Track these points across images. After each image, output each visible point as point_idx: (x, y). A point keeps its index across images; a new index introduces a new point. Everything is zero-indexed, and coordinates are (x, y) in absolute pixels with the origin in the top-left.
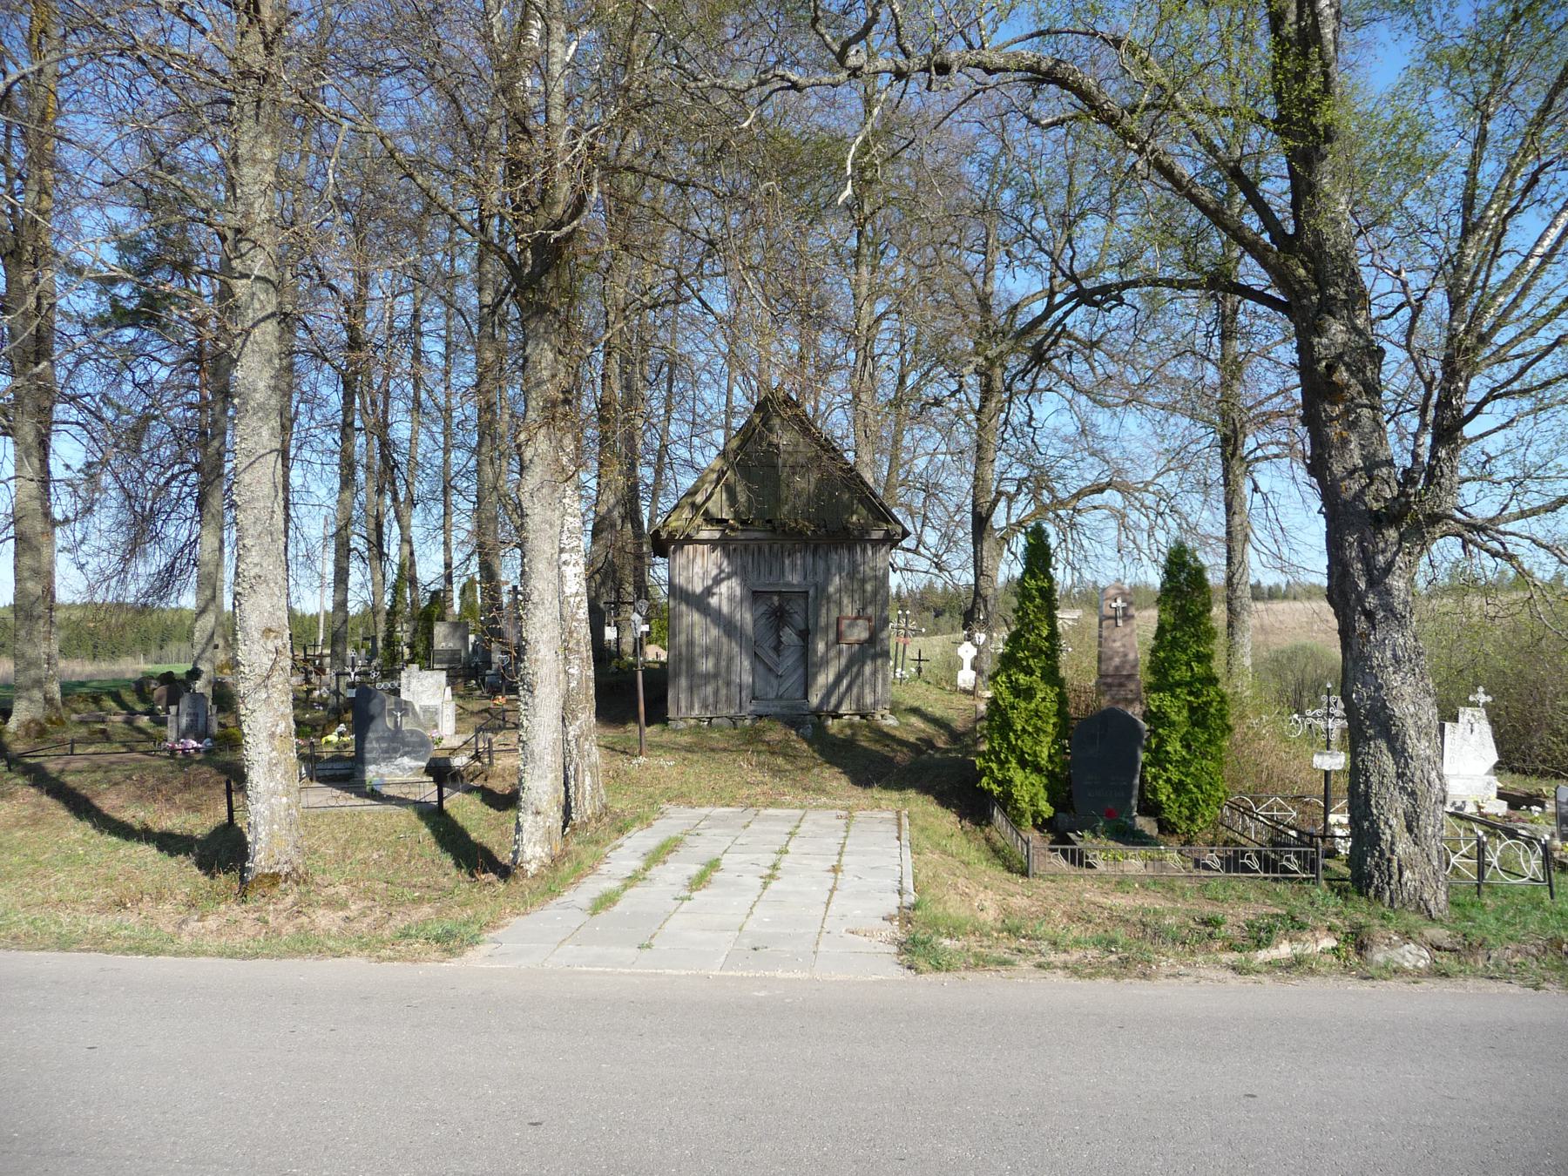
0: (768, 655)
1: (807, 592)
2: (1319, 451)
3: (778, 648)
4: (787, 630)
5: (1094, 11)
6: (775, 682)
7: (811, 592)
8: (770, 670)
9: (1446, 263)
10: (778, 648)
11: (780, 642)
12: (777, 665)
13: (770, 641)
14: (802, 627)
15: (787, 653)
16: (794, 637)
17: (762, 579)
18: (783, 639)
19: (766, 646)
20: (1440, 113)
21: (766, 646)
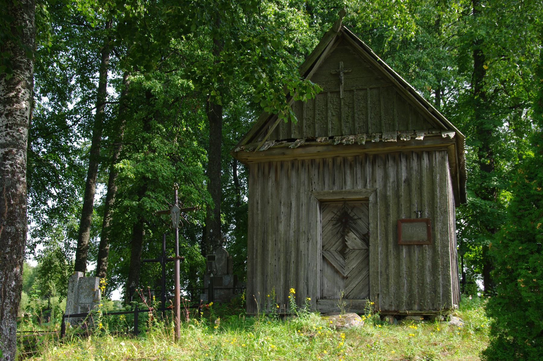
0: (337, 260)
1: (367, 199)
2: (407, 88)
3: (343, 251)
4: (352, 235)
5: (493, 359)
6: (341, 283)
7: (371, 199)
8: (337, 272)
9: (507, 165)
10: (343, 251)
11: (345, 246)
12: (343, 267)
13: (337, 245)
14: (366, 231)
15: (352, 256)
16: (359, 241)
17: (326, 189)
18: (349, 243)
19: (332, 249)
20: (71, 52)
21: (332, 249)
